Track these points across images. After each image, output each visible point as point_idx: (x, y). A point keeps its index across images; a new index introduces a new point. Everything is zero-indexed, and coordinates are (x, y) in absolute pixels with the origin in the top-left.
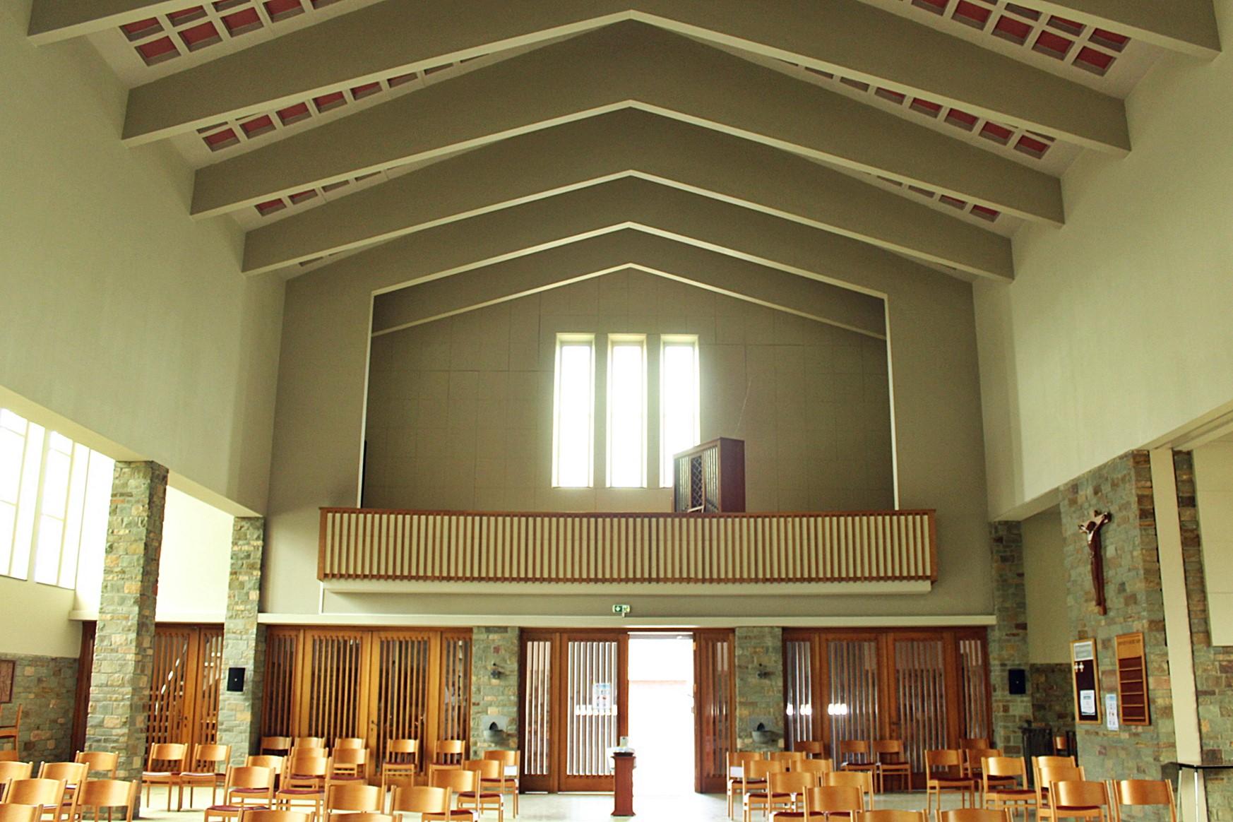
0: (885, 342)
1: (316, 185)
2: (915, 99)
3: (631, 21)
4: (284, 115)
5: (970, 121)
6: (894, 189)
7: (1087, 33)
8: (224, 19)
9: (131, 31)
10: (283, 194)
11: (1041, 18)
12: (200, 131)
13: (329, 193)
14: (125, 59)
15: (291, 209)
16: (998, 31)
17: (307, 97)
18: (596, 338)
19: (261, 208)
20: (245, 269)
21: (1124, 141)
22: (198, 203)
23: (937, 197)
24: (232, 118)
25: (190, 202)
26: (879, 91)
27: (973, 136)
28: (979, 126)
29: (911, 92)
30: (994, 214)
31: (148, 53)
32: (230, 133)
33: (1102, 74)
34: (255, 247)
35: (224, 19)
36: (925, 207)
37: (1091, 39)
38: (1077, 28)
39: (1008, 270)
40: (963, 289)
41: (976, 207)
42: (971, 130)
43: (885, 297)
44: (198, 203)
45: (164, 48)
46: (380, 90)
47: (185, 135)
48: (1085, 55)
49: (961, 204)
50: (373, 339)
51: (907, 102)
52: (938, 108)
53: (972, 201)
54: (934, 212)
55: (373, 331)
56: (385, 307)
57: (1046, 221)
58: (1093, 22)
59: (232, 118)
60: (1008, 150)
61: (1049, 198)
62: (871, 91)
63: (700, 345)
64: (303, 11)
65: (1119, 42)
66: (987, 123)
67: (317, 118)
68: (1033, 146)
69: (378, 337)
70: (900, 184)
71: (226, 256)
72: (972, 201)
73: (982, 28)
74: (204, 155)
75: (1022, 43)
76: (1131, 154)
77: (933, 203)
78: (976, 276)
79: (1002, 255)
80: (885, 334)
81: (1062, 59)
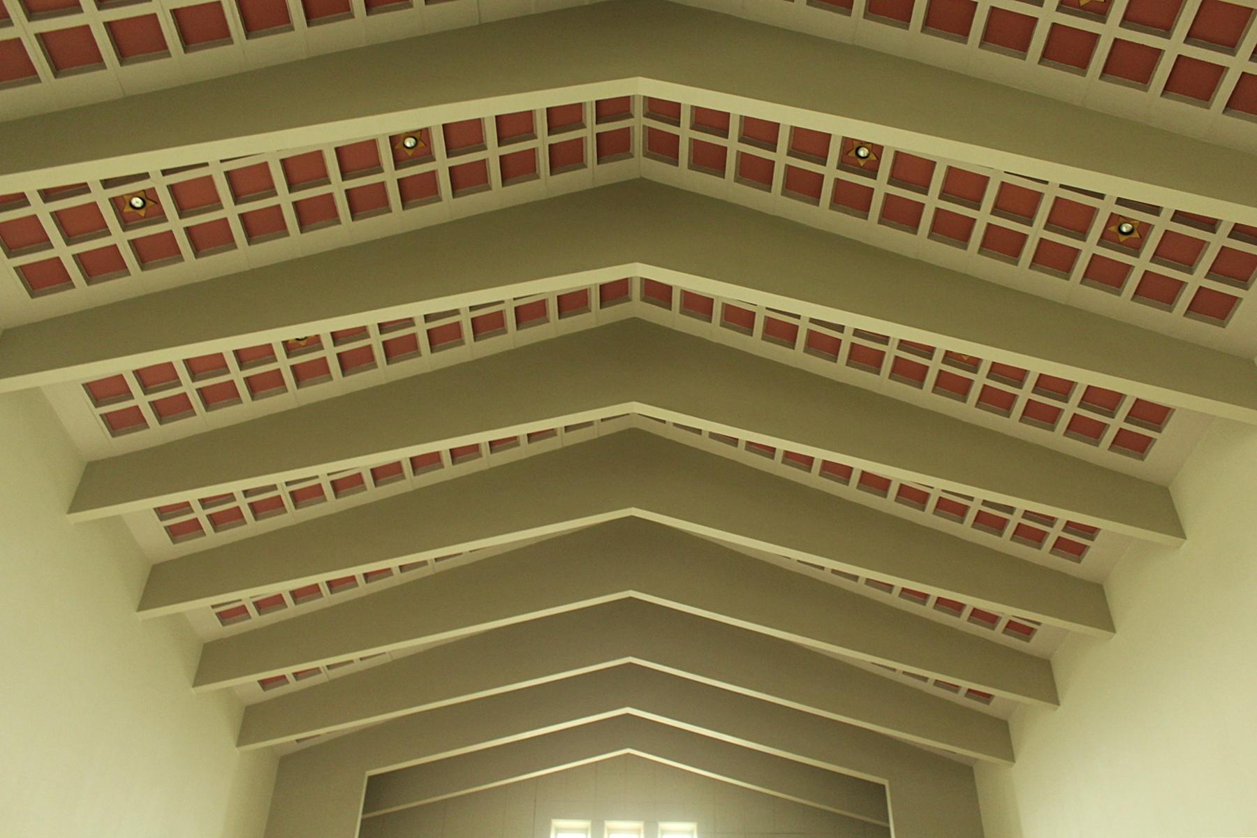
0: (888, 829)
1: (321, 663)
2: (903, 589)
3: (631, 598)
4: (295, 594)
5: (957, 608)
6: (888, 674)
7: (1224, 230)
8: (200, 391)
9: (162, 512)
10: (288, 671)
11: (1016, 513)
12: (213, 607)
13: (334, 671)
14: (86, 424)
15: (294, 686)
16: (1088, 280)
17: (321, 579)
18: (593, 825)
19: (264, 684)
20: (239, 745)
21: (1176, 528)
22: (202, 676)
23: (931, 682)
24: (246, 596)
25: (194, 672)
26: (869, 582)
27: (962, 622)
28: (966, 613)
29: (899, 583)
30: (987, 697)
31: (116, 424)
32: (243, 610)
33: (1079, 562)
34: (252, 722)
35: (200, 391)
36: (920, 691)
37: (1065, 530)
38: (1050, 521)
39: (1009, 754)
40: (964, 773)
41: (969, 690)
42: (959, 616)
43: (885, 782)
44: (202, 676)
45: (133, 420)
46: (392, 574)
47: (200, 611)
48: (1060, 544)
49: (955, 688)
50: (363, 820)
51: (896, 591)
52: (926, 596)
53: (965, 685)
54: (927, 695)
55: (364, 812)
56: (375, 783)
57: (1043, 703)
58: (1064, 515)
59: (246, 596)
60: (997, 634)
61: (1042, 679)
62: (861, 582)
63: (699, 833)
64: (325, 500)
65: (1091, 532)
66: (975, 609)
67: (328, 599)
68: (1021, 630)
69: (369, 819)
70: (894, 670)
71: (225, 735)
72: (965, 685)
73: (962, 522)
74: (214, 629)
75: (1000, 535)
76: (1060, 709)
77: (928, 688)
78: (976, 760)
79: (1000, 737)
80: (888, 821)
81: (1040, 548)
